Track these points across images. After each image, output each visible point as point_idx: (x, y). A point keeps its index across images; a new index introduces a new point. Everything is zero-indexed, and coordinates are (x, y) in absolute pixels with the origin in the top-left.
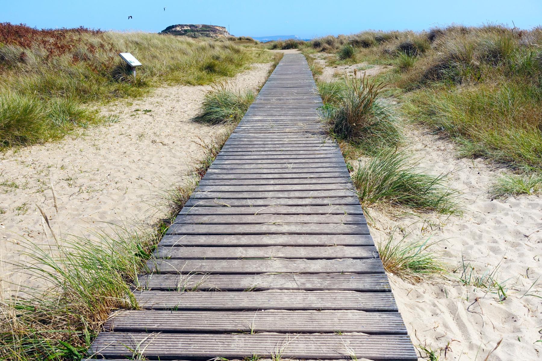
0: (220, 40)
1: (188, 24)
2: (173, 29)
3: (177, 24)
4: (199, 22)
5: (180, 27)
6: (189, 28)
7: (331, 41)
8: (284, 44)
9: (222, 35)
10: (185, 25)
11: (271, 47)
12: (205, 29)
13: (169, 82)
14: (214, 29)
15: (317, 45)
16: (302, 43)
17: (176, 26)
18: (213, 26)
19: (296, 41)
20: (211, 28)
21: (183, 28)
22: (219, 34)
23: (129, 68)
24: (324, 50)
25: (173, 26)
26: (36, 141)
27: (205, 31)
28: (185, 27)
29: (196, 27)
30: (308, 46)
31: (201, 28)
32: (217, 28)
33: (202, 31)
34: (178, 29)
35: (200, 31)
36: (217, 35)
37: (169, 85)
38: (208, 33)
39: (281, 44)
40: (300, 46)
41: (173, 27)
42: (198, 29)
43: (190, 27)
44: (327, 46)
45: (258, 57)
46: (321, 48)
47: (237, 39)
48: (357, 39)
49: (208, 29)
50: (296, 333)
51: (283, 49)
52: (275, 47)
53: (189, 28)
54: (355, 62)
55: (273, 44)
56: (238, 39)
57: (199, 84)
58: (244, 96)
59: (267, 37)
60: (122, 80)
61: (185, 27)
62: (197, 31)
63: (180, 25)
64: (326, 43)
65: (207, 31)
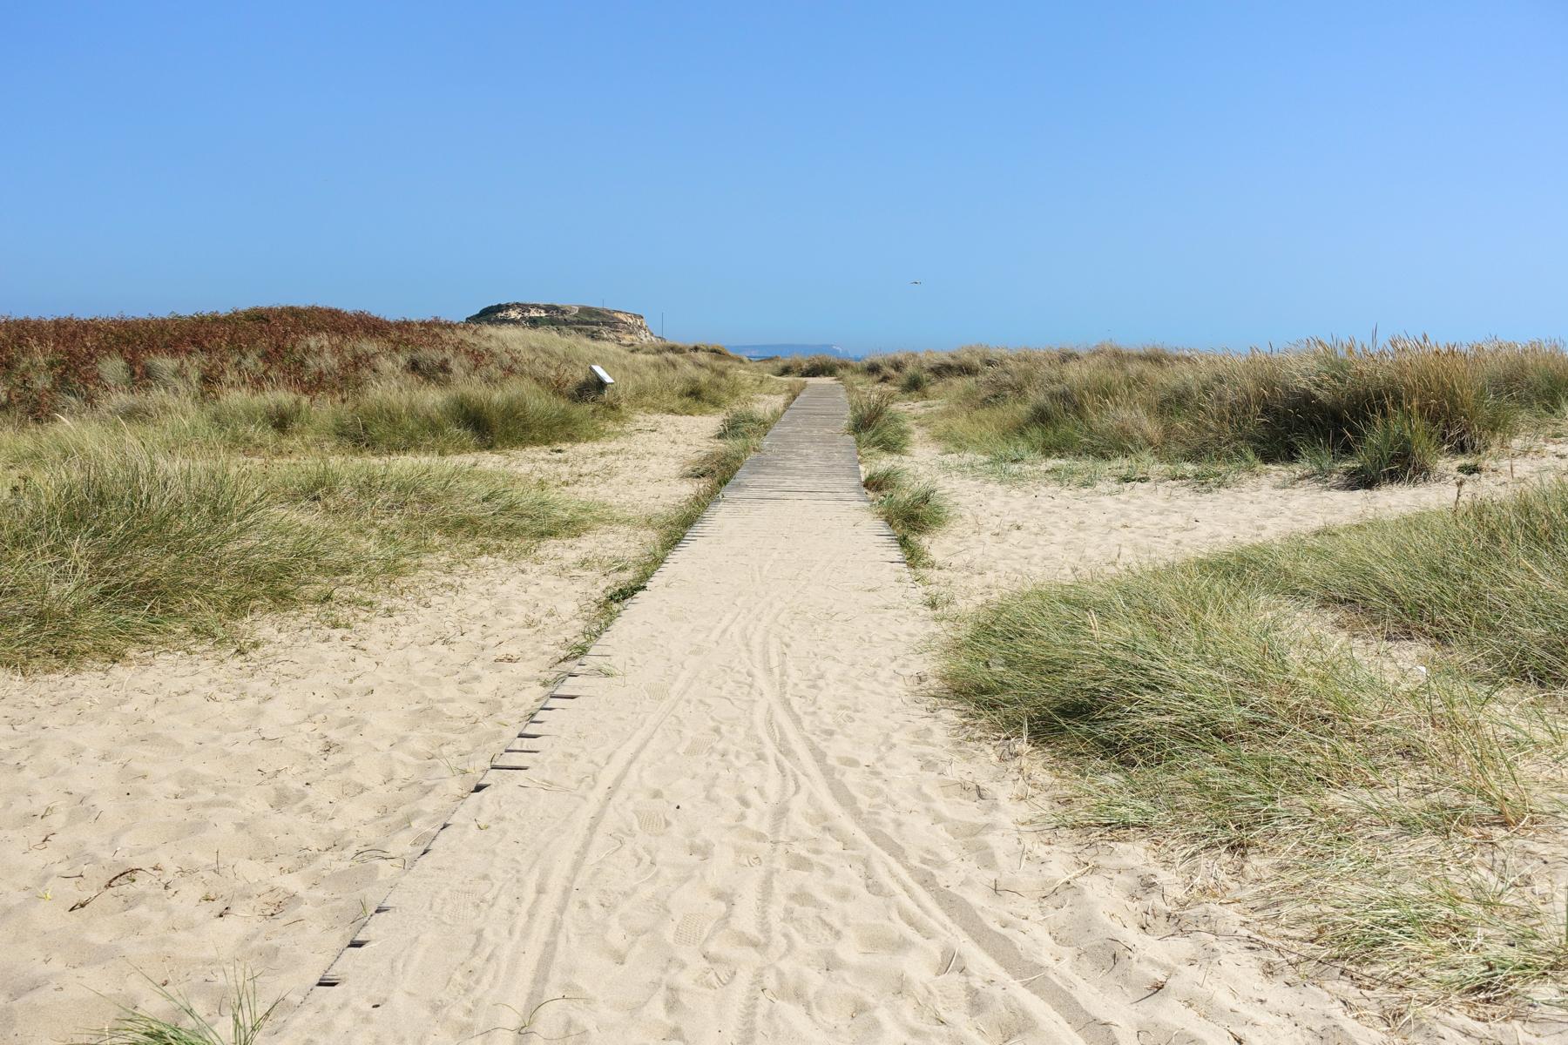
0: (645, 349)
1: (541, 303)
2: (500, 315)
3: (511, 301)
4: (572, 300)
5: (518, 310)
6: (543, 315)
7: (901, 363)
8: (805, 366)
9: (634, 337)
10: (533, 306)
11: (776, 370)
12: (588, 319)
13: (645, 408)
14: (613, 318)
15: (873, 369)
16: (845, 366)
17: (508, 307)
18: (609, 311)
19: (833, 359)
20: (604, 316)
21: (526, 314)
22: (624, 332)
23: (601, 385)
24: (885, 379)
25: (499, 306)
26: (579, 441)
27: (587, 323)
28: (532, 310)
29: (564, 312)
30: (857, 372)
31: (576, 316)
32: (621, 316)
33: (578, 323)
34: (513, 314)
35: (572, 323)
36: (619, 334)
37: (646, 412)
38: (595, 328)
39: (800, 365)
40: (841, 372)
41: (499, 308)
42: (566, 317)
43: (547, 312)
44: (893, 372)
45: (758, 386)
46: (881, 377)
47: (687, 350)
48: (951, 362)
49: (594, 320)
50: (853, 800)
51: (803, 376)
52: (786, 371)
53: (543, 315)
54: (925, 396)
55: (780, 364)
56: (691, 350)
57: (688, 414)
58: (769, 415)
59: (754, 347)
60: (593, 400)
61: (532, 310)
62: (566, 323)
63: (518, 305)
64: (892, 366)
65: (592, 324)
